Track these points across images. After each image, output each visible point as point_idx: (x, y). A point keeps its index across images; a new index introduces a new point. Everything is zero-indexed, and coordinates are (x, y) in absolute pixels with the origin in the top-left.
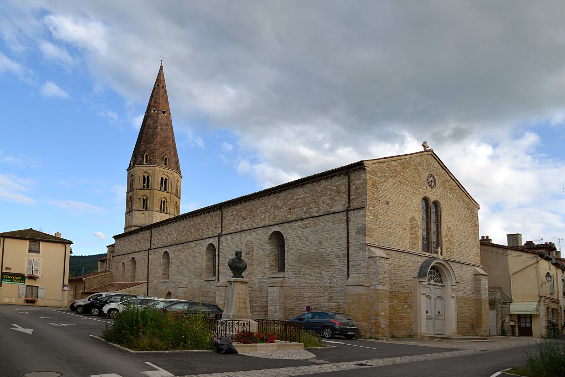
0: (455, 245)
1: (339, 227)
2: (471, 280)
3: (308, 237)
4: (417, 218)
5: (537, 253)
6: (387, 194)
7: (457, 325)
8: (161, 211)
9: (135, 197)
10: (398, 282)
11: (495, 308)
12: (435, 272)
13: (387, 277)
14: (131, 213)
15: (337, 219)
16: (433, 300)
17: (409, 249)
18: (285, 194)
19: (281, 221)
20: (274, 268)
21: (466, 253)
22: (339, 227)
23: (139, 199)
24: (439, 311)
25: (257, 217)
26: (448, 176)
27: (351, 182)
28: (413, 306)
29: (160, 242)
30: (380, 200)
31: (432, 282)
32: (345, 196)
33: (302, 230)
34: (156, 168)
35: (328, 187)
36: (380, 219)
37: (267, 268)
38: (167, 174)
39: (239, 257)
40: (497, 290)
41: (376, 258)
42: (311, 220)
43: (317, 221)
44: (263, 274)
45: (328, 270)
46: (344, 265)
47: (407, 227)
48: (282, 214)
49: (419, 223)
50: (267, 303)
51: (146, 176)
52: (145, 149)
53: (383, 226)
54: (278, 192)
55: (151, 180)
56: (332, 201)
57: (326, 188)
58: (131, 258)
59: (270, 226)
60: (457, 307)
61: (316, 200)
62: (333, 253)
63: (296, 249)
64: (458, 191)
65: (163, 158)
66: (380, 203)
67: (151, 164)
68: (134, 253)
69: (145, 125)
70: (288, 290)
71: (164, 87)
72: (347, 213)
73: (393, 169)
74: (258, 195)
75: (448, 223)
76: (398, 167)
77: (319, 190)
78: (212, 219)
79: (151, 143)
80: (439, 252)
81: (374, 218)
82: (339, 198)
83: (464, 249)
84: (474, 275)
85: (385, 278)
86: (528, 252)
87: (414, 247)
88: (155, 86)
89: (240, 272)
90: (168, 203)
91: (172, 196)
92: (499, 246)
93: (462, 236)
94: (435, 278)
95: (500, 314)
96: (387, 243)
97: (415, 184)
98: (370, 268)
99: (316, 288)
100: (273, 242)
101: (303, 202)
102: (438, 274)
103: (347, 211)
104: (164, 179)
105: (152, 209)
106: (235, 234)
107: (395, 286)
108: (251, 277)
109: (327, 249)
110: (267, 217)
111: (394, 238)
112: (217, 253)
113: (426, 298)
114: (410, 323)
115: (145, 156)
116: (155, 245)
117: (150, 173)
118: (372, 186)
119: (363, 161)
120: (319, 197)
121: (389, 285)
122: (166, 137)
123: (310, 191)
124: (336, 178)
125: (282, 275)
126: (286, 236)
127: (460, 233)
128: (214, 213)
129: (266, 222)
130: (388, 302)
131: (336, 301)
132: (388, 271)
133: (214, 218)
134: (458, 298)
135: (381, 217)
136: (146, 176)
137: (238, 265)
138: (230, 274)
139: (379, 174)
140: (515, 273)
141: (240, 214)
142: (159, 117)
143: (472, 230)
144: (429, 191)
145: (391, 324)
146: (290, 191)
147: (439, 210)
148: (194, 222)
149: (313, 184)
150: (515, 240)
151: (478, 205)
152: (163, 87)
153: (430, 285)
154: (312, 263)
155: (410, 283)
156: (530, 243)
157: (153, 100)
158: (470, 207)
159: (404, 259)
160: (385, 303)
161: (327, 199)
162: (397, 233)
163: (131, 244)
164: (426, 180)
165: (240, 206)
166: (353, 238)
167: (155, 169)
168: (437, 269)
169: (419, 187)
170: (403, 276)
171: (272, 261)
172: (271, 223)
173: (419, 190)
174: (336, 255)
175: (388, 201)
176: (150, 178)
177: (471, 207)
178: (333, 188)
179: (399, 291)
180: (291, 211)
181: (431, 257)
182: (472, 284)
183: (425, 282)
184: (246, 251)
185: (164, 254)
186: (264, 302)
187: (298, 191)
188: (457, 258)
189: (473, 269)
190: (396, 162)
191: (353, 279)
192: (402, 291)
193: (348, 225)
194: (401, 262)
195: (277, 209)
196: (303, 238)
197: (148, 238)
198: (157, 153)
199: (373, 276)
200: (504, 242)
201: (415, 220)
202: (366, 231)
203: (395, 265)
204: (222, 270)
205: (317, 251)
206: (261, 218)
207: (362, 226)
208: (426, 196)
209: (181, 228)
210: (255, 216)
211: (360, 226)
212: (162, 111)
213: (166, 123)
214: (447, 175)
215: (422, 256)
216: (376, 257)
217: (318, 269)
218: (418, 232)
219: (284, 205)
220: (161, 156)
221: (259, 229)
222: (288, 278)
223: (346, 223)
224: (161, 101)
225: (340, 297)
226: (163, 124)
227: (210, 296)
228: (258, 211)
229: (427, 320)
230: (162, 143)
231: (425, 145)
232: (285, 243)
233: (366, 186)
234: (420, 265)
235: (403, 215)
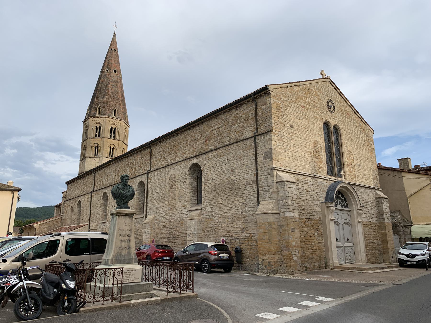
0: (356, 169)
1: (248, 153)
2: (374, 204)
3: (221, 167)
4: (321, 143)
5: (429, 174)
6: (291, 118)
7: (365, 252)
8: (110, 157)
10: (307, 208)
11: (397, 232)
12: (340, 196)
14: (84, 161)
15: (246, 146)
16: (341, 226)
17: (315, 173)
20: (193, 200)
21: (366, 177)
22: (248, 153)
24: (347, 238)
26: (345, 102)
27: (258, 108)
29: (102, 184)
30: (285, 124)
31: (339, 207)
32: (253, 122)
33: (217, 159)
34: (107, 118)
35: (238, 116)
36: (285, 143)
37: (187, 201)
38: (116, 123)
39: (125, 182)
40: (397, 213)
41: (283, 183)
42: (224, 149)
44: (184, 207)
46: (254, 192)
47: (311, 151)
48: (200, 146)
49: (322, 147)
51: (98, 126)
52: (98, 103)
53: (289, 150)
55: (102, 130)
56: (242, 129)
57: (236, 117)
58: (78, 201)
59: (190, 158)
61: (228, 130)
62: (244, 180)
63: (212, 179)
64: (354, 117)
72: (255, 139)
75: (348, 147)
76: (300, 92)
77: (230, 119)
78: (143, 157)
79: (104, 98)
82: (248, 125)
83: (364, 173)
85: (293, 203)
86: (421, 174)
87: (319, 171)
88: (109, 50)
89: (126, 200)
91: (120, 143)
92: (394, 169)
94: (342, 203)
95: (403, 238)
96: (293, 167)
97: (316, 109)
100: (192, 175)
101: (217, 133)
103: (255, 137)
104: (114, 128)
105: (102, 155)
106: (161, 169)
107: (304, 212)
108: (174, 211)
109: (238, 177)
111: (300, 162)
112: (146, 189)
113: (335, 224)
114: (322, 253)
115: (98, 108)
116: (97, 187)
117: (101, 123)
118: (277, 110)
119: (268, 86)
120: (231, 126)
121: (297, 211)
122: (116, 92)
123: (222, 121)
124: (245, 106)
125: (200, 207)
126: (203, 167)
127: (359, 156)
128: (145, 152)
129: (187, 156)
130: (299, 230)
131: (248, 231)
133: (145, 156)
134: (364, 224)
135: (286, 141)
136: (98, 126)
137: (122, 192)
140: (411, 196)
142: (110, 75)
144: (329, 116)
145: (303, 254)
146: (206, 124)
147: (339, 134)
149: (226, 114)
150: (406, 164)
151: (372, 129)
152: (115, 50)
153: (338, 211)
154: (226, 192)
155: (318, 209)
156: (417, 167)
157: (107, 62)
158: (366, 132)
160: (295, 231)
161: (237, 127)
162: (303, 157)
163: (79, 188)
164: (326, 105)
165: (166, 143)
166: (261, 164)
168: (342, 194)
170: (311, 201)
171: (191, 193)
172: (191, 156)
173: (320, 114)
174: (246, 182)
175: (293, 125)
176: (101, 127)
178: (242, 116)
179: (308, 218)
180: (207, 142)
181: (336, 180)
182: (375, 208)
183: (332, 207)
184: (170, 186)
185: (104, 195)
187: (213, 122)
188: (359, 182)
189: (374, 193)
190: (298, 87)
191: (263, 206)
192: (311, 217)
193: (256, 150)
194: (308, 186)
195: (196, 142)
199: (281, 202)
200: (396, 165)
202: (273, 155)
204: (150, 206)
205: (229, 180)
206: (182, 152)
208: (327, 120)
209: (118, 169)
211: (267, 150)
214: (344, 101)
216: (284, 181)
217: (231, 198)
218: (322, 155)
221: (180, 162)
223: (254, 149)
224: (113, 62)
225: (252, 227)
226: (114, 81)
227: (139, 234)
228: (180, 146)
229: (338, 249)
231: (322, 73)
232: (202, 174)
235: (307, 139)
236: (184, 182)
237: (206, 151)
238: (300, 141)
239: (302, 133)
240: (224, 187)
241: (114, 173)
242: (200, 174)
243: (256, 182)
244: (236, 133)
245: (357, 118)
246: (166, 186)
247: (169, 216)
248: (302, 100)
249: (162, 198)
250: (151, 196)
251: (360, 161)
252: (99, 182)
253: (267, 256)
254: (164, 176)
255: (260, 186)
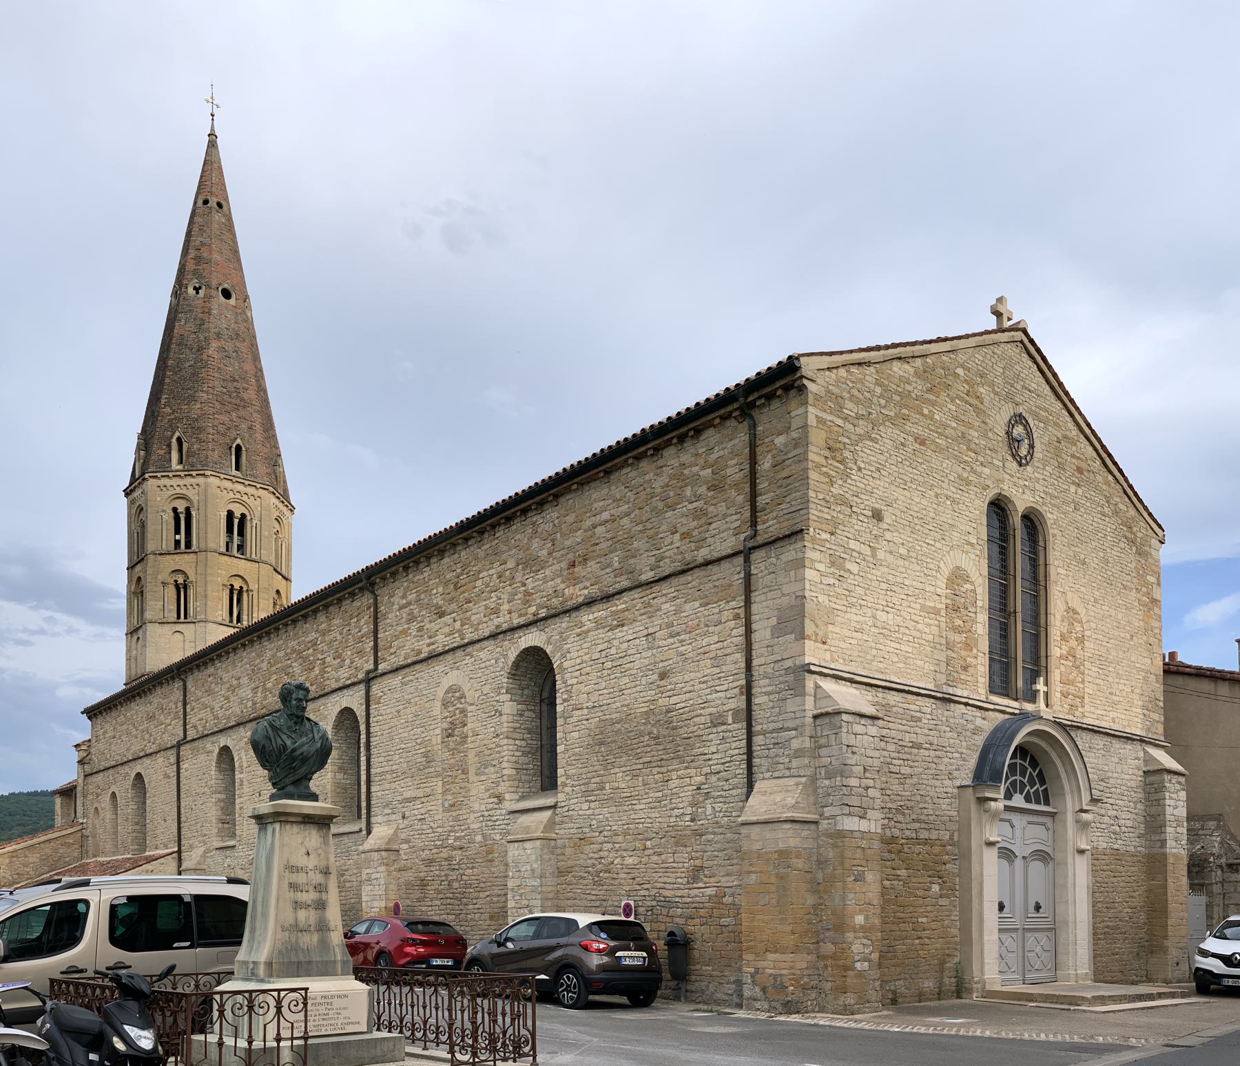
1: (720, 612)
2: (1135, 792)
4: (974, 576)
6: (878, 482)
8: (231, 621)
9: (149, 578)
10: (909, 804)
11: (1202, 885)
12: (1026, 764)
13: (874, 787)
14: (140, 634)
15: (715, 586)
16: (1018, 863)
17: (946, 684)
18: (557, 515)
19: (545, 610)
20: (527, 778)
21: (1121, 699)
22: (720, 612)
23: (164, 584)
24: (1037, 903)
25: (475, 604)
26: (1071, 425)
27: (758, 442)
28: (958, 887)
29: (210, 717)
30: (854, 504)
32: (740, 498)
33: (610, 634)
34: (212, 480)
35: (686, 472)
36: (852, 576)
37: (505, 778)
38: (245, 498)
41: (837, 718)
42: (636, 596)
43: (654, 598)
44: (496, 800)
45: (689, 770)
49: (979, 590)
50: (506, 902)
51: (181, 509)
52: (175, 419)
53: (864, 603)
54: (536, 509)
57: (679, 477)
58: (133, 775)
59: (513, 630)
60: (1091, 885)
61: (649, 525)
62: (703, 708)
63: (590, 704)
65: (230, 448)
66: (853, 516)
67: (193, 467)
68: (141, 758)
69: (171, 339)
70: (568, 851)
71: (225, 208)
72: (747, 560)
73: (896, 392)
74: (476, 526)
75: (1069, 595)
76: (914, 385)
77: (657, 485)
78: (349, 624)
79: (193, 398)
80: (1042, 694)
81: (832, 570)
82: (722, 508)
83: (1116, 686)
84: (1144, 772)
85: (867, 788)
87: (962, 677)
88: (195, 203)
89: (303, 771)
90: (251, 594)
91: (262, 572)
93: (1110, 639)
94: (1028, 787)
96: (875, 663)
97: (969, 449)
98: (820, 756)
99: (649, 840)
100: (523, 689)
102: (1035, 774)
103: (746, 553)
104: (237, 514)
105: (203, 617)
106: (412, 668)
107: (900, 818)
108: (460, 812)
109: (683, 697)
110: (506, 600)
111: (897, 646)
114: (948, 948)
116: (195, 727)
118: (827, 453)
119: (797, 358)
120: (659, 513)
122: (237, 377)
123: (629, 494)
124: (711, 436)
125: (550, 801)
126: (558, 662)
129: (501, 620)
130: (878, 877)
131: (712, 880)
132: (877, 763)
133: (355, 620)
134: (1096, 855)
135: (854, 568)
136: (181, 509)
137: (289, 742)
138: (400, 806)
139: (850, 408)
141: (426, 600)
142: (210, 309)
143: (1141, 618)
145: (887, 955)
146: (568, 501)
147: (1041, 543)
148: (300, 640)
149: (641, 465)
152: (220, 205)
153: (1012, 814)
154: (639, 751)
157: (192, 253)
159: (932, 722)
161: (683, 515)
162: (910, 626)
163: (134, 732)
164: (1002, 433)
165: (427, 572)
167: (207, 485)
169: (981, 459)
170: (925, 782)
171: (520, 754)
173: (979, 469)
174: (711, 714)
176: (194, 513)
177: (1140, 535)
178: (702, 473)
179: (914, 835)
180: (574, 572)
181: (1017, 712)
183: (995, 800)
184: (445, 725)
186: (499, 895)
187: (594, 496)
189: (1141, 754)
192: (924, 835)
194: (919, 731)
196: (608, 665)
197: (176, 708)
198: (211, 431)
199: (827, 782)
201: (967, 580)
202: (807, 622)
203: (901, 743)
204: (379, 794)
205: (652, 707)
206: (486, 607)
207: (793, 602)
208: (1003, 493)
209: (264, 665)
210: (470, 602)
211: (785, 600)
212: (220, 289)
213: (233, 329)
214: (1069, 419)
215: (987, 710)
216: (839, 713)
217: (655, 770)
218: (974, 621)
219: (554, 554)
220: (222, 440)
222: (566, 808)
223: (743, 597)
225: (723, 866)
227: (348, 885)
228: (479, 583)
229: (1004, 936)
230: (226, 397)
231: (1001, 309)
233: (806, 452)
234: (980, 740)
235: (929, 560)
236: (493, 713)
237: (570, 603)
238: (904, 570)
239: (911, 539)
240: (633, 733)
241: (250, 679)
242: (547, 688)
243: (744, 715)
244: (677, 536)
245: (1110, 486)
246: (431, 727)
247: (445, 829)
248: (917, 416)
249: (422, 768)
250: (381, 759)
251: (1105, 644)
252: (201, 710)
253: (771, 956)
254: (424, 692)
255: (757, 728)
